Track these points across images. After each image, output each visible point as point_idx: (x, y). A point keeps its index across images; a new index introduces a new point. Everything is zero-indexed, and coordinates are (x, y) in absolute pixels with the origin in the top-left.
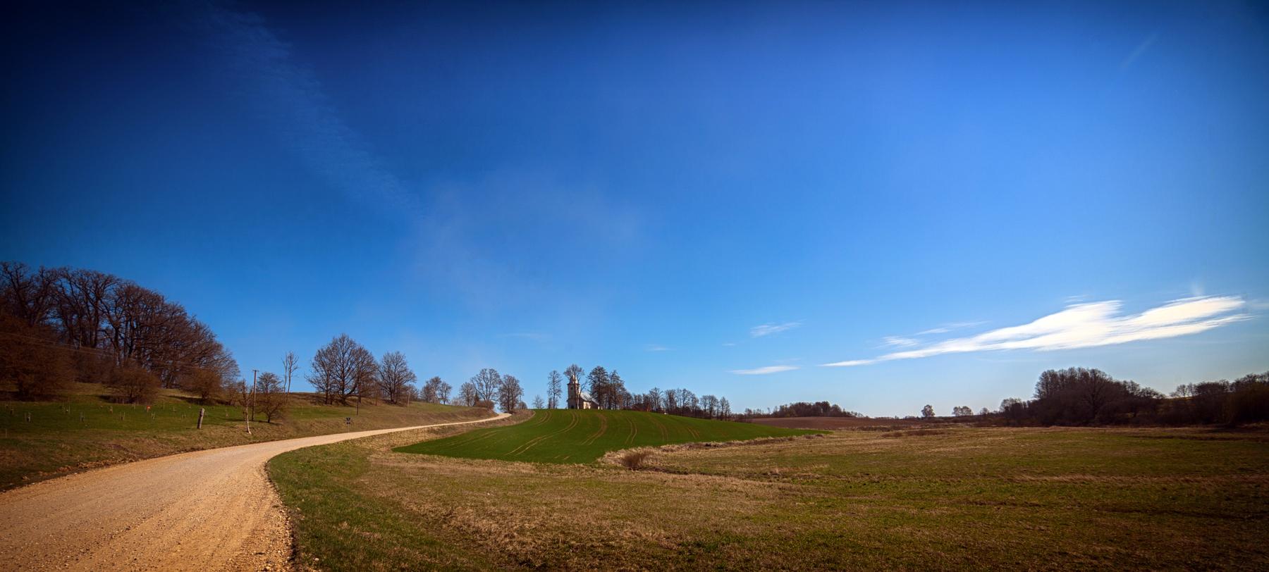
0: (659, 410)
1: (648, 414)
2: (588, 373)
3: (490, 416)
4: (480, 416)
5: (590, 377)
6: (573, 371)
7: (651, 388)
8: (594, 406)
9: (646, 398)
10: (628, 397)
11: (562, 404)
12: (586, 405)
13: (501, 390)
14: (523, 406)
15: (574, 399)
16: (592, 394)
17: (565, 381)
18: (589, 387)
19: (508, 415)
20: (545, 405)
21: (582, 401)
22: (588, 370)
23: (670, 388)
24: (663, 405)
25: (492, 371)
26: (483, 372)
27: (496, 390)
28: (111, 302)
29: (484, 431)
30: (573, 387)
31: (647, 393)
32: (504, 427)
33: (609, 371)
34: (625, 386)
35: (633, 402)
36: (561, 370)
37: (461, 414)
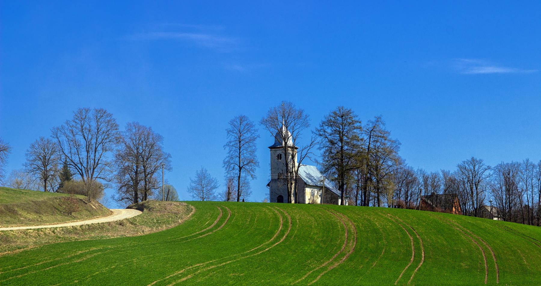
0: (480, 212)
1: (453, 220)
2: (315, 122)
3: (92, 214)
4: (69, 213)
5: (321, 133)
6: (284, 117)
7: (465, 157)
8: (329, 198)
9: (451, 182)
10: (408, 179)
11: (258, 192)
12: (311, 195)
13: (120, 157)
14: (169, 195)
15: (285, 187)
16: (324, 171)
17: (265, 139)
18: (318, 153)
19: (134, 213)
20: (219, 193)
21: (301, 185)
22: (317, 114)
23: (508, 160)
24: (489, 200)
25: (101, 113)
26: (81, 116)
27: (109, 157)
28: (124, 130)
29: (78, 244)
30: (280, 151)
31: (453, 169)
32: (124, 239)
33: (364, 118)
34: (401, 154)
35: (419, 191)
36: (256, 115)
37: (26, 208)
